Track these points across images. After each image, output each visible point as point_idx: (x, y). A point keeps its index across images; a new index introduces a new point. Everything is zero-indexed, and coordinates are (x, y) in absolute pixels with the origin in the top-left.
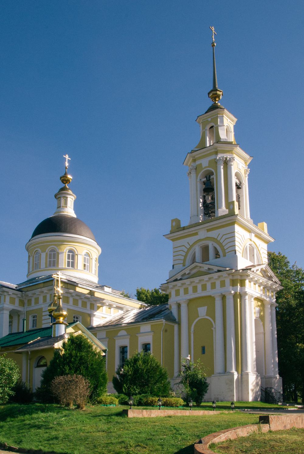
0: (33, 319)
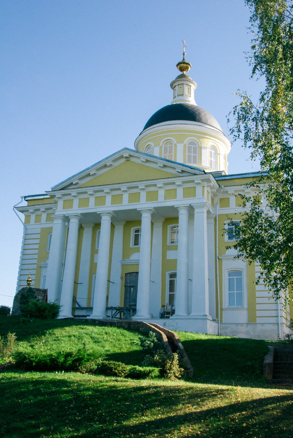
0: (139, 233)
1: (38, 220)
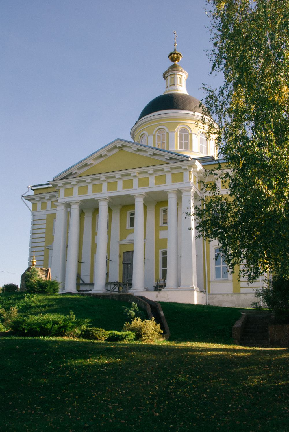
1: (44, 206)
